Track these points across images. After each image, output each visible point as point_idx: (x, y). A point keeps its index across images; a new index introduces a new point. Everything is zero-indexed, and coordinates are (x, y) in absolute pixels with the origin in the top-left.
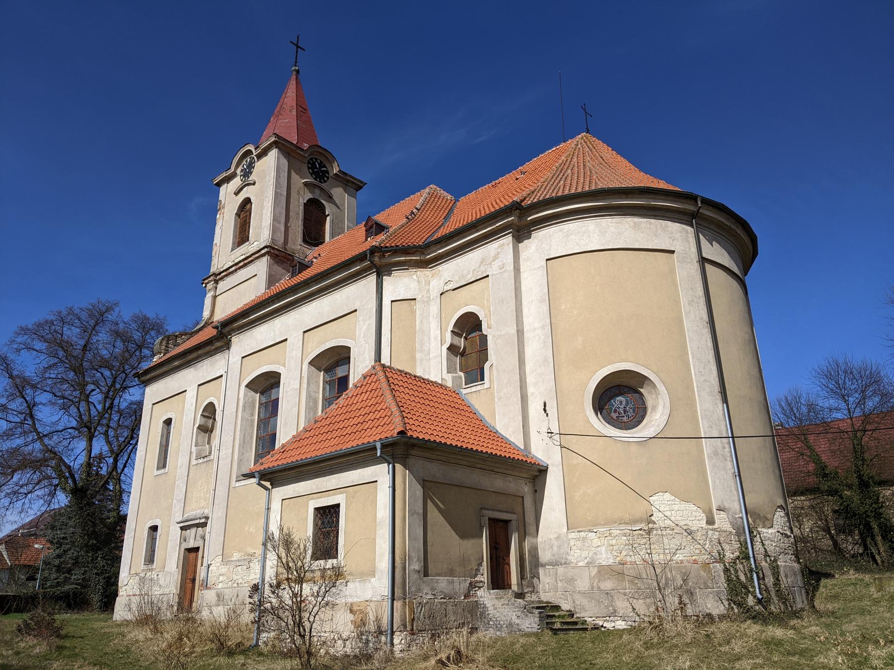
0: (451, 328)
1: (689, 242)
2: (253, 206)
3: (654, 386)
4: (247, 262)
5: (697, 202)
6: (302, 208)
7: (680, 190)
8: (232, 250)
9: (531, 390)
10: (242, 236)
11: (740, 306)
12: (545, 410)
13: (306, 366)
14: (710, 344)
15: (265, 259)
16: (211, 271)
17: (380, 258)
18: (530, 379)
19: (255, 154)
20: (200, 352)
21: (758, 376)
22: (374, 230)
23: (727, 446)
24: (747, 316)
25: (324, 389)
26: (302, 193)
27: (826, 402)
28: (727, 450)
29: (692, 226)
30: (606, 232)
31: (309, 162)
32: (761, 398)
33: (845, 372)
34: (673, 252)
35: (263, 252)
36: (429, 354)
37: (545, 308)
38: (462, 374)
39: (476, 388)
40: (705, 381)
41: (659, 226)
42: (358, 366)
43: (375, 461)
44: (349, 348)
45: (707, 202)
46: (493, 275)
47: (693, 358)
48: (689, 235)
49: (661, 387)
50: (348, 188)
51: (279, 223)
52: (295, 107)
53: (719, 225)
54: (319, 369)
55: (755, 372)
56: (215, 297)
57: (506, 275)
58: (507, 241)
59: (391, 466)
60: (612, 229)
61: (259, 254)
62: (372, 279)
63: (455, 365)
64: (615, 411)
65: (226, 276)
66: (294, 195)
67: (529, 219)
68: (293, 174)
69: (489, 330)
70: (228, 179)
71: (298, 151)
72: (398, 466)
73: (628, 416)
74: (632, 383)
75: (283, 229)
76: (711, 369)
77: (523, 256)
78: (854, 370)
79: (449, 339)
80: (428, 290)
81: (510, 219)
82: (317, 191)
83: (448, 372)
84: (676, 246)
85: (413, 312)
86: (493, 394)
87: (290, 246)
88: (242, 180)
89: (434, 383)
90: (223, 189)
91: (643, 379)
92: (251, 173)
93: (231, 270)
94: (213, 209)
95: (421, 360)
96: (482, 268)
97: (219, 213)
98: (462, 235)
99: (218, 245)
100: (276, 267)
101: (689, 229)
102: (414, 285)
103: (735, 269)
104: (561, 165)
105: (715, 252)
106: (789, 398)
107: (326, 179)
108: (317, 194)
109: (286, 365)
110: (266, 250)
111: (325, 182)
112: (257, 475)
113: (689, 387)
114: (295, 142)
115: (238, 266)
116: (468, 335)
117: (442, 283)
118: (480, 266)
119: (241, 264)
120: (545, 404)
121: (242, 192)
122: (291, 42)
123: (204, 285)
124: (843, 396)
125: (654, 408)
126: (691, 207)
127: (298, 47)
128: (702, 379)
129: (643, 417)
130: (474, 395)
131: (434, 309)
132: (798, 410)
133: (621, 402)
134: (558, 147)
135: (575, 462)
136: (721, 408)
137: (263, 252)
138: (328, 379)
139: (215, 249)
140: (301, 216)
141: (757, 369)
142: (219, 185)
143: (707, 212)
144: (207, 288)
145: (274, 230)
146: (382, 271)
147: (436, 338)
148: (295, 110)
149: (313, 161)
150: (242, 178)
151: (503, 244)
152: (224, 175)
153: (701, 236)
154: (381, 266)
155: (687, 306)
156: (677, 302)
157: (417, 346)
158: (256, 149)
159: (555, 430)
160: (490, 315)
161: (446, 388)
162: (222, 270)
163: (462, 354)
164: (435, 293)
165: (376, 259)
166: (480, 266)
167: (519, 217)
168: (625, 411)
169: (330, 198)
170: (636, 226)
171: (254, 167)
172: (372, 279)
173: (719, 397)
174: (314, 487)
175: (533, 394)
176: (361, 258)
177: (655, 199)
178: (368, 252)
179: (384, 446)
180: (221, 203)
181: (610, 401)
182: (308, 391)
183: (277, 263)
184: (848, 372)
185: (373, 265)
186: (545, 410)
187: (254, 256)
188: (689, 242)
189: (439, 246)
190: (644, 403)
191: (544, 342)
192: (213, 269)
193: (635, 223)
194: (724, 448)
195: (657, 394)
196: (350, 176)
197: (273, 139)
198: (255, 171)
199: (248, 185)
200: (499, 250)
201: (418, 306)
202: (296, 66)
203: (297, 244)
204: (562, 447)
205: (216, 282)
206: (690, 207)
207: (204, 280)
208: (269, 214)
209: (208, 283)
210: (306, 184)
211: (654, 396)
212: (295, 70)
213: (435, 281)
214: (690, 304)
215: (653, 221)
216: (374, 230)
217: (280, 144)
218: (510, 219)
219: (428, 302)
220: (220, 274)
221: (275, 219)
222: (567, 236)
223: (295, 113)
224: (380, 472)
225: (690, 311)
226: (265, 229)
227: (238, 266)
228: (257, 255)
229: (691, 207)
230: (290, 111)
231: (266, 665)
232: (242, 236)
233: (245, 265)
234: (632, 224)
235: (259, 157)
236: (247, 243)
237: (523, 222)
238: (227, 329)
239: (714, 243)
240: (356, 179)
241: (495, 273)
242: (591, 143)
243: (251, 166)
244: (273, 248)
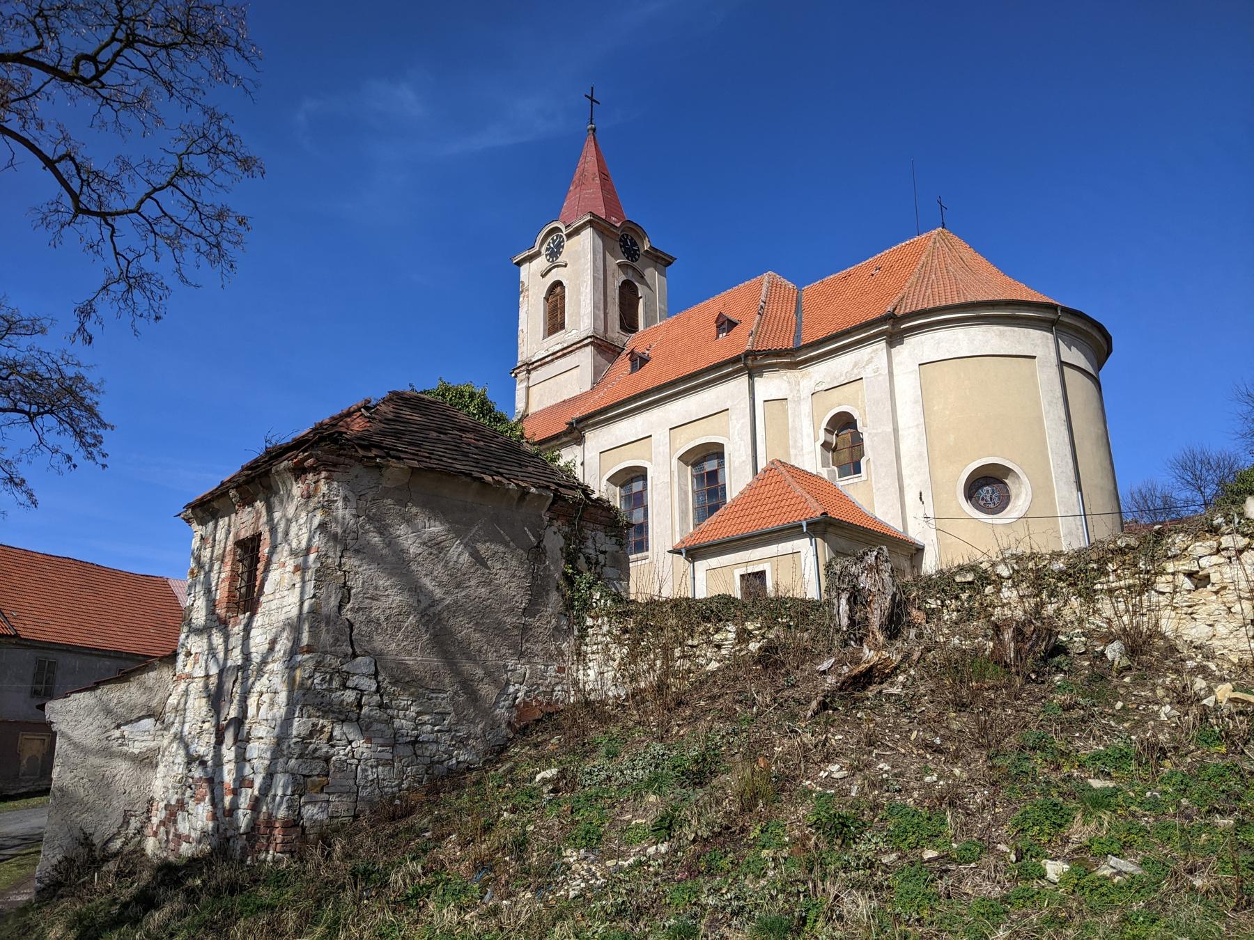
0: (824, 425)
1: (1048, 347)
2: (566, 290)
3: (1018, 477)
4: (566, 352)
5: (1057, 311)
6: (617, 291)
8: (544, 338)
9: (906, 482)
10: (555, 322)
11: (1095, 403)
12: (921, 499)
13: (675, 461)
14: (1067, 440)
15: (589, 349)
16: (519, 359)
17: (752, 361)
18: (905, 472)
19: (565, 233)
21: (1109, 467)
22: (725, 326)
23: (1080, 527)
24: (1100, 412)
25: (692, 482)
26: (616, 275)
27: (1183, 494)
28: (1080, 530)
29: (1052, 332)
30: (974, 340)
31: (621, 240)
32: (1111, 487)
33: (1202, 462)
34: (1034, 357)
35: (586, 342)
36: (802, 450)
37: (920, 409)
38: (836, 468)
39: (852, 480)
40: (1062, 472)
41: (1022, 334)
42: (734, 462)
43: (801, 535)
44: (722, 445)
45: (1064, 310)
46: (866, 378)
47: (1052, 453)
48: (1049, 341)
49: (1024, 478)
50: (658, 265)
51: (599, 310)
52: (597, 174)
53: (1078, 330)
54: (687, 464)
55: (1107, 464)
56: (528, 388)
57: (881, 378)
58: (881, 345)
59: (813, 540)
60: (980, 337)
61: (581, 344)
62: (744, 380)
63: (828, 459)
64: (983, 499)
65: (541, 365)
66: (610, 279)
67: (902, 327)
68: (608, 255)
69: (865, 428)
70: (530, 259)
71: (612, 229)
72: (818, 539)
73: (994, 503)
74: (997, 474)
75: (602, 316)
76: (1067, 462)
77: (895, 360)
78: (1211, 460)
79: (822, 436)
80: (799, 390)
81: (885, 327)
82: (630, 272)
83: (823, 467)
84: (1038, 352)
85: (785, 411)
86: (870, 485)
87: (610, 334)
88: (548, 260)
89: (811, 474)
90: (524, 270)
91: (1007, 471)
92: (560, 253)
93: (547, 360)
94: (514, 290)
95: (796, 455)
96: (856, 371)
97: (522, 295)
99: (525, 331)
100: (599, 357)
101: (1049, 335)
102: (785, 385)
103: (1091, 370)
104: (922, 267)
105: (1074, 356)
106: (1143, 491)
107: (637, 257)
108: (631, 276)
109: (653, 459)
110: (589, 340)
111: (637, 260)
112: (683, 551)
113: (1048, 478)
114: (604, 217)
115: (555, 356)
116: (839, 432)
117: (812, 384)
118: (853, 369)
119: (558, 354)
120: (921, 493)
121: (550, 274)
122: (586, 96)
123: (513, 375)
124: (1199, 488)
125: (1018, 496)
126: (1051, 316)
127: (593, 100)
128: (1060, 470)
129: (1007, 504)
130: (852, 487)
131: (806, 407)
132: (1152, 501)
133: (988, 491)
134: (912, 241)
135: (949, 541)
136: (1076, 496)
137: (586, 342)
138: (695, 474)
139: (521, 335)
140: (617, 300)
141: (1108, 462)
142: (519, 264)
143: (1066, 319)
144: (517, 379)
145: (595, 318)
146: (754, 372)
147: (808, 436)
148: (598, 179)
150: (548, 257)
151: (877, 350)
152: (527, 253)
153: (1060, 341)
154: (753, 368)
155: (1047, 406)
156: (1038, 403)
157: (791, 443)
158: (566, 227)
159: (931, 514)
160: (865, 414)
161: (823, 479)
162: (533, 360)
163: (834, 450)
164: (806, 393)
165: (750, 362)
166: (853, 369)
167: (893, 325)
168: (991, 499)
169: (642, 277)
170: (1001, 334)
171: (563, 247)
172: (744, 380)
173: (1074, 486)
174: (738, 558)
175: (909, 485)
176: (736, 360)
177: (1019, 310)
178: (742, 356)
179: (808, 524)
180: (523, 285)
181: (977, 490)
182: (679, 484)
183: (599, 353)
184: (1206, 463)
185: (746, 366)
186: (921, 499)
187: (575, 346)
188: (1048, 347)
190: (1008, 492)
191: (919, 440)
192: (522, 358)
193: (1000, 331)
194: (1078, 529)
195: (1021, 483)
196: (661, 252)
197: (588, 218)
198: (565, 251)
199: (558, 266)
200: (873, 355)
201: (790, 406)
202: (591, 123)
203: (615, 333)
204: (937, 530)
205: (529, 372)
206: (1050, 315)
207: (514, 370)
208: (588, 301)
209: (519, 373)
210: (620, 265)
211: (1017, 486)
212: (591, 129)
213: (805, 381)
214: (1049, 405)
215: (1016, 329)
216: (725, 326)
217: (595, 223)
218: (885, 327)
219: (798, 401)
220: (533, 363)
221: (595, 307)
222: (939, 343)
223: (598, 182)
224: (804, 546)
226: (585, 317)
227: (555, 356)
228: (578, 345)
229: (1051, 316)
230: (593, 179)
232: (555, 322)
233: (564, 355)
234: (997, 332)
235: (569, 236)
236: (564, 331)
237: (896, 330)
238: (581, 425)
239: (1073, 348)
240: (666, 255)
241: (869, 376)
242: (949, 241)
243: (559, 246)
244: (597, 338)
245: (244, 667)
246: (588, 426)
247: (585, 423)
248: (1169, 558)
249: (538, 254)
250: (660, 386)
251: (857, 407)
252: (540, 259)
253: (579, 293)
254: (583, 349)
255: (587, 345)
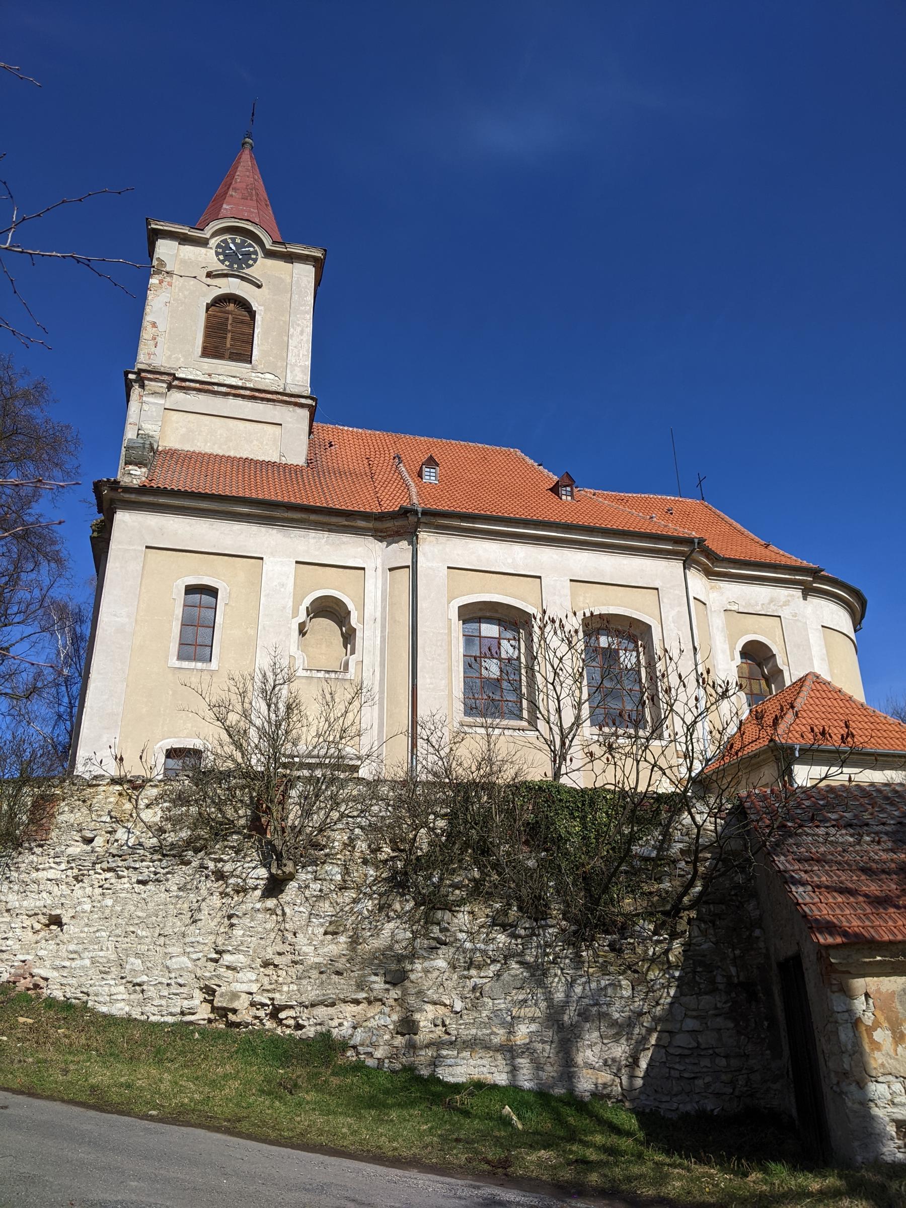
0: (307, 602)
7: (811, 565)
13: (738, 656)
20: (313, 517)
61: (293, 399)
98: (760, 568)
115: (233, 391)
149: (253, 259)
150: (251, 262)
152: (185, 230)
179: (800, 750)
189: (732, 565)
197: (318, 254)
205: (170, 387)
225: (449, 1034)
227: (233, 391)
231: (305, 1085)
245: (256, 746)
246: (429, 525)
247: (433, 520)
248: (130, 781)
249: (203, 243)
250: (608, 529)
251: (775, 643)
252: (202, 250)
253: (285, 333)
254: (291, 408)
255: (302, 406)
